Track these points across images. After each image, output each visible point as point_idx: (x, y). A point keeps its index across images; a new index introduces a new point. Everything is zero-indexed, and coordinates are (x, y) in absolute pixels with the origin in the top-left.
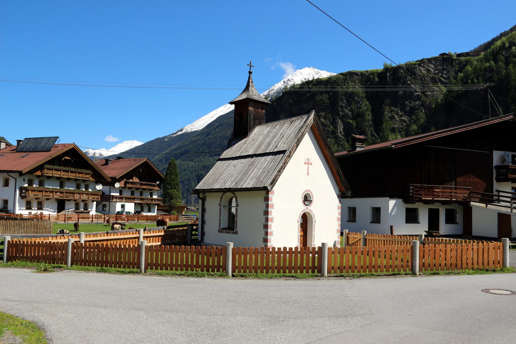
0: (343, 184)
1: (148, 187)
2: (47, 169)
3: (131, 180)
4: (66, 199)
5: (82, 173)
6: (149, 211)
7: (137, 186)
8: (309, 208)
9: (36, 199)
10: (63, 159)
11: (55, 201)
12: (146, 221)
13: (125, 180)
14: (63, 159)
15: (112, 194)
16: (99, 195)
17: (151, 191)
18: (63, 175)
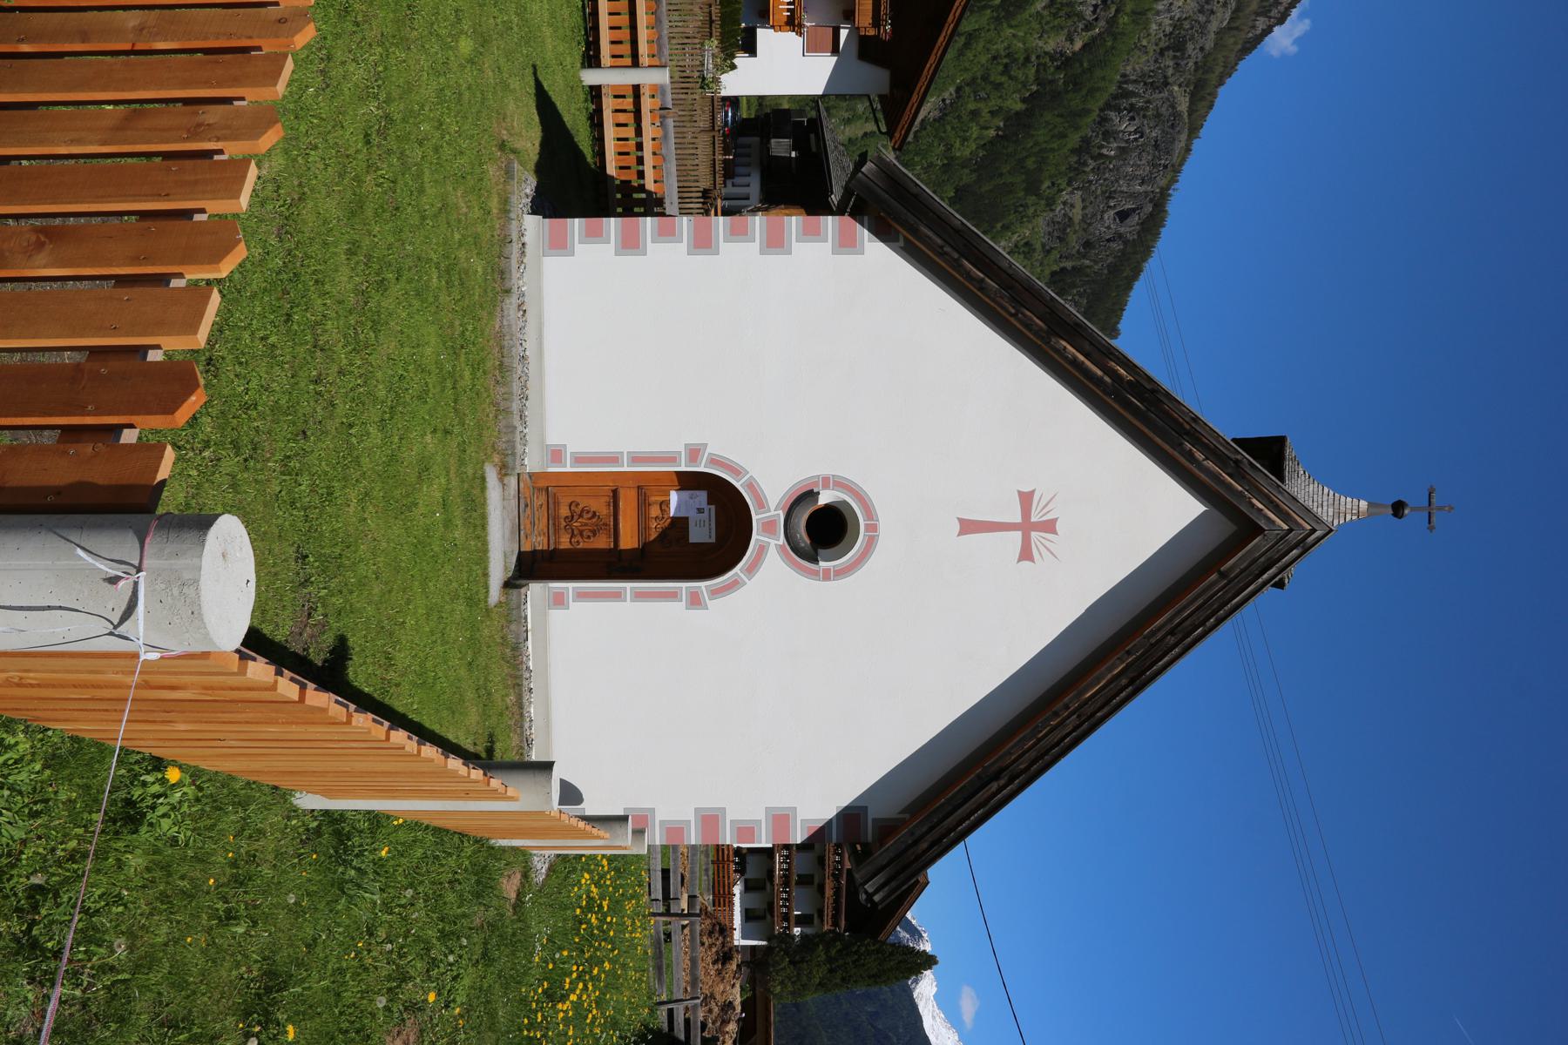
0: (931, 829)
1: (831, 901)
6: (748, 916)
8: (773, 542)
12: (711, 858)
17: (816, 916)
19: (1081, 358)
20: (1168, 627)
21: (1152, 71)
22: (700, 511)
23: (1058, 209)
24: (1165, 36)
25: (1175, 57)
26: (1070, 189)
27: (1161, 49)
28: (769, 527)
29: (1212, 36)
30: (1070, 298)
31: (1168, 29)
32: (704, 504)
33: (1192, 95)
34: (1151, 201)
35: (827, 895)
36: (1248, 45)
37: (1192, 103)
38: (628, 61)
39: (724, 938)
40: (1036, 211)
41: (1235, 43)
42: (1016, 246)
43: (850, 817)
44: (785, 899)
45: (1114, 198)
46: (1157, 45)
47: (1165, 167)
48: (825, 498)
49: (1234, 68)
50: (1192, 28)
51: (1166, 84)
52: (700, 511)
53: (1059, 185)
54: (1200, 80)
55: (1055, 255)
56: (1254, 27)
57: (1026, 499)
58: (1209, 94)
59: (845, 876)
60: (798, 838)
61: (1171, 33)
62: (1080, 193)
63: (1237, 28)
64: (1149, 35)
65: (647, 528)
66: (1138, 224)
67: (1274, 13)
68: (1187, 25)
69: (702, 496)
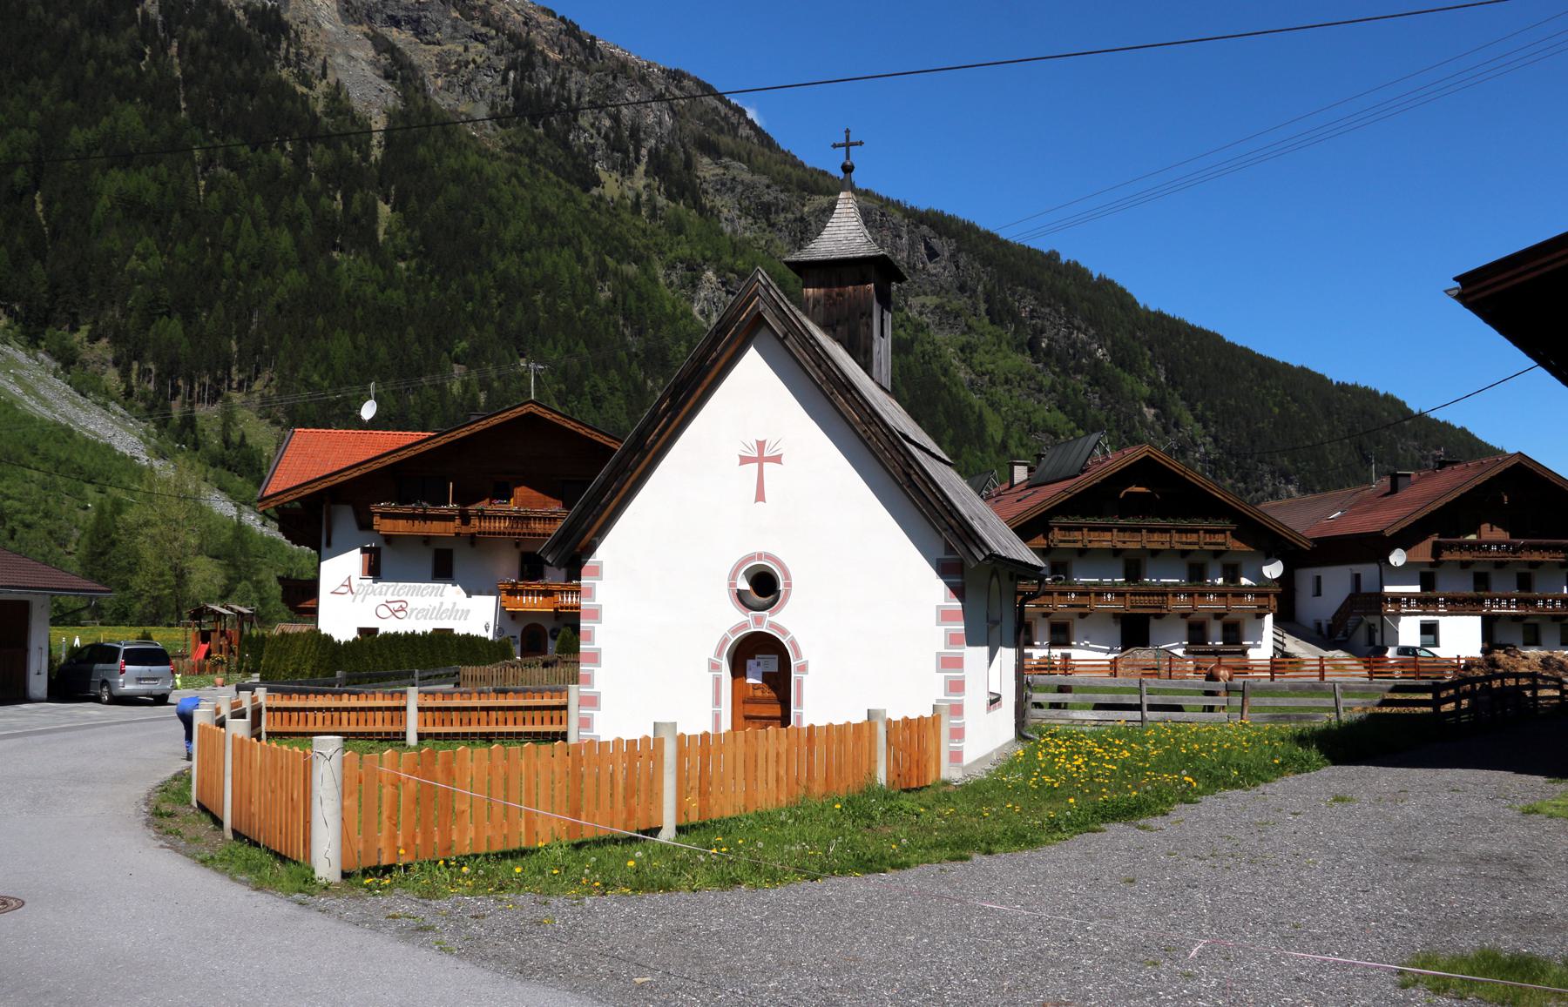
1: (1546, 554)
2: (1061, 528)
3: (1473, 537)
4: (1152, 614)
5: (1196, 531)
7: (1491, 555)
8: (768, 618)
9: (1046, 615)
10: (1122, 495)
11: (1112, 620)
13: (1435, 538)
14: (1122, 495)
15: (1388, 589)
16: (1272, 596)
18: (1090, 541)
19: (657, 430)
20: (816, 369)
21: (790, 233)
22: (759, 664)
23: (927, 320)
24: (756, 223)
25: (777, 212)
26: (907, 309)
27: (769, 226)
28: (758, 621)
29: (756, 177)
30: (1017, 304)
31: (750, 220)
32: (755, 662)
33: (812, 192)
34: (917, 227)
35: (1540, 559)
36: (765, 142)
37: (820, 192)
38: (564, 712)
39: (1474, 666)
40: (929, 343)
41: (763, 155)
42: (964, 361)
43: (943, 570)
44: (1545, 602)
45: (915, 264)
46: (764, 231)
47: (883, 215)
48: (744, 585)
49: (787, 154)
50: (749, 197)
51: (802, 219)
52: (759, 664)
53: (902, 320)
54: (798, 186)
55: (973, 321)
56: (748, 138)
57: (744, 460)
58: (812, 176)
59: (1515, 541)
60: (957, 604)
61: (754, 217)
62: (910, 298)
63: (749, 155)
64: (755, 239)
65: (769, 698)
66: (940, 239)
67: (734, 120)
68: (746, 203)
69: (750, 663)
